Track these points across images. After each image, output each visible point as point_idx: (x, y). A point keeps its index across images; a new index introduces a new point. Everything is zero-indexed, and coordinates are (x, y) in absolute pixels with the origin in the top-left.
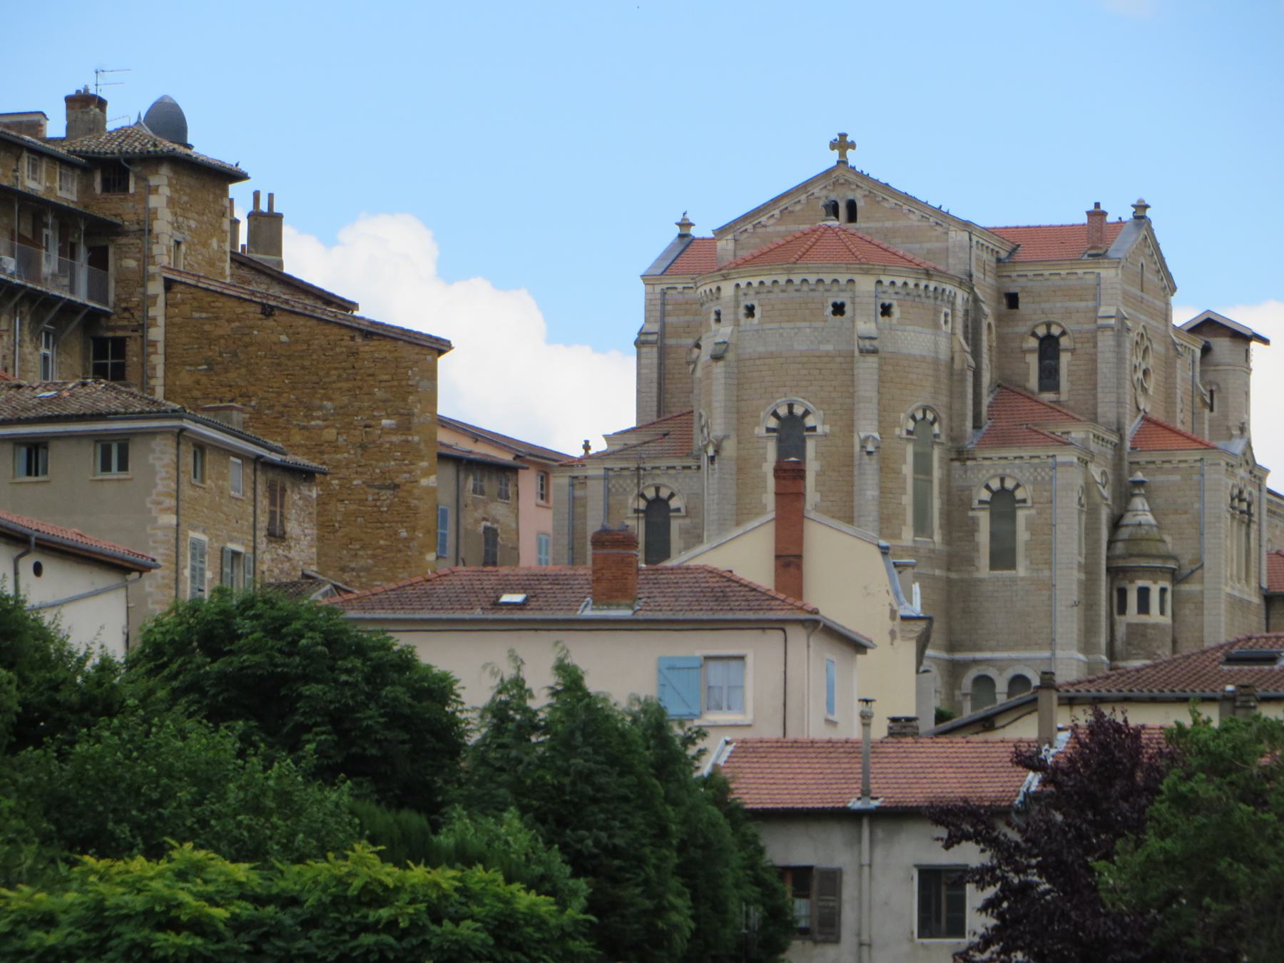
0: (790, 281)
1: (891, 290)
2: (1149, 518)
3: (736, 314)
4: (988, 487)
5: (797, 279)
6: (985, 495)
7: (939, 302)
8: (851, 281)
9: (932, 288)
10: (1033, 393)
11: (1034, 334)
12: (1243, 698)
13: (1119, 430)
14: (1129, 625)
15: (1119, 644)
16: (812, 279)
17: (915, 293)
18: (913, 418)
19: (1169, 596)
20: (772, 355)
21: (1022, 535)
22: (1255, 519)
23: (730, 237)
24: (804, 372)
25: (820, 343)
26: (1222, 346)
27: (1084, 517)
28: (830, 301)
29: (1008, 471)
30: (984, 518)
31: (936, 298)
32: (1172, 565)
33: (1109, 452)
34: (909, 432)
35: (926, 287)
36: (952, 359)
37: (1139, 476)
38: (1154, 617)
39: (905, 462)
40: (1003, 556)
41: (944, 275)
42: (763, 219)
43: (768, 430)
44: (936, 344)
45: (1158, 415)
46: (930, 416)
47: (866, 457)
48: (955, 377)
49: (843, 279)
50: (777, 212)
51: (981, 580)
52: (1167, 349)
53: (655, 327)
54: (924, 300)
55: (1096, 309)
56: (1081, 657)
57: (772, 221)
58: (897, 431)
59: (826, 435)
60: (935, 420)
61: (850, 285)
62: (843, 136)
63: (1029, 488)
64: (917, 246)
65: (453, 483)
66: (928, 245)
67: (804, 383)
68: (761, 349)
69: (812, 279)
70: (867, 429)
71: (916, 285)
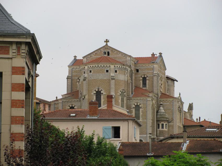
1: (117, 68)
2: (163, 111)
4: (134, 105)
5: (100, 66)
8: (110, 66)
9: (124, 67)
11: (141, 77)
14: (159, 131)
16: (102, 65)
18: (121, 91)
19: (167, 125)
20: (95, 80)
21: (141, 114)
28: (106, 70)
29: (138, 102)
31: (125, 69)
32: (168, 120)
34: (120, 94)
35: (123, 67)
36: (128, 81)
37: (161, 103)
38: (165, 129)
42: (92, 55)
43: (94, 93)
46: (124, 91)
49: (108, 66)
50: (94, 54)
53: (71, 75)
54: (123, 70)
55: (153, 72)
59: (105, 94)
63: (142, 105)
66: (123, 60)
69: (102, 65)
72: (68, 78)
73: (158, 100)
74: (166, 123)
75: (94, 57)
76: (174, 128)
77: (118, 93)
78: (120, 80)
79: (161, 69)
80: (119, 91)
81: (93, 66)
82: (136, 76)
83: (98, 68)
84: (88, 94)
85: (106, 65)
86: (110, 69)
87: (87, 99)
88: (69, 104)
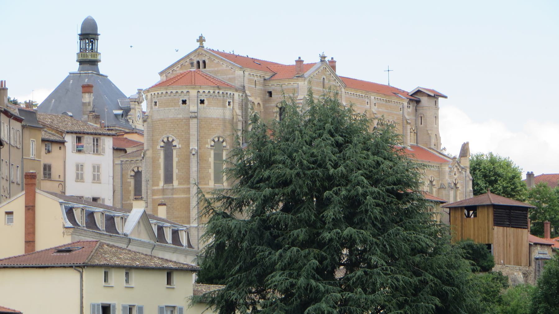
0: (167, 93)
1: (204, 94)
3: (151, 105)
5: (169, 92)
8: (188, 92)
9: (229, 94)
11: (277, 106)
17: (214, 95)
18: (214, 141)
20: (162, 120)
23: (164, 75)
24: (172, 125)
25: (178, 114)
31: (224, 96)
35: (218, 92)
36: (233, 118)
39: (210, 157)
41: (231, 87)
42: (175, 68)
43: (161, 147)
44: (224, 113)
46: (221, 140)
47: (192, 156)
49: (185, 91)
50: (179, 66)
54: (218, 97)
57: (178, 69)
58: (207, 146)
59: (180, 148)
61: (188, 94)
64: (225, 76)
68: (159, 117)
69: (174, 91)
70: (194, 146)
71: (214, 92)
77: (207, 143)
80: (209, 140)
81: (177, 92)
83: (168, 97)
86: (189, 98)
88: (133, 166)
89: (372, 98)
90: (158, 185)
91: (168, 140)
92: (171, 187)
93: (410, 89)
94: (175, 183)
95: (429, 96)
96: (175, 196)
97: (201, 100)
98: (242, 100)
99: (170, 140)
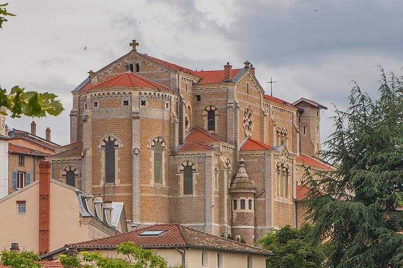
1: (145, 96)
2: (246, 175)
4: (182, 165)
5: (111, 93)
6: (182, 168)
7: (164, 100)
9: (161, 95)
10: (205, 131)
11: (206, 110)
12: (71, 253)
13: (236, 144)
15: (234, 220)
16: (116, 92)
18: (154, 141)
19: (253, 202)
20: (103, 120)
21: (195, 182)
22: (290, 174)
25: (119, 115)
26: (307, 110)
27: (218, 175)
28: (123, 100)
29: (190, 159)
30: (182, 176)
32: (253, 191)
33: (231, 152)
34: (152, 146)
35: (158, 94)
36: (170, 119)
37: (242, 160)
38: (247, 210)
40: (188, 190)
43: (102, 146)
45: (257, 138)
46: (161, 140)
48: (172, 126)
49: (127, 92)
51: (181, 198)
52: (261, 114)
53: (76, 110)
55: (227, 100)
56: (217, 225)
60: (163, 142)
62: (134, 41)
63: (197, 165)
65: (32, 165)
66: (163, 79)
67: (114, 130)
69: (116, 92)
72: (73, 115)
73: (236, 154)
74: (249, 198)
75: (112, 74)
76: (266, 208)
78: (151, 119)
79: (248, 93)
82: (196, 109)
84: (92, 146)
85: (118, 92)
87: (89, 157)
89: (271, 106)
90: (99, 184)
91: (109, 140)
92: (113, 186)
93: (292, 100)
94: (117, 182)
95: (312, 106)
96: (116, 194)
97: (142, 101)
98: (177, 102)
99: (112, 139)
